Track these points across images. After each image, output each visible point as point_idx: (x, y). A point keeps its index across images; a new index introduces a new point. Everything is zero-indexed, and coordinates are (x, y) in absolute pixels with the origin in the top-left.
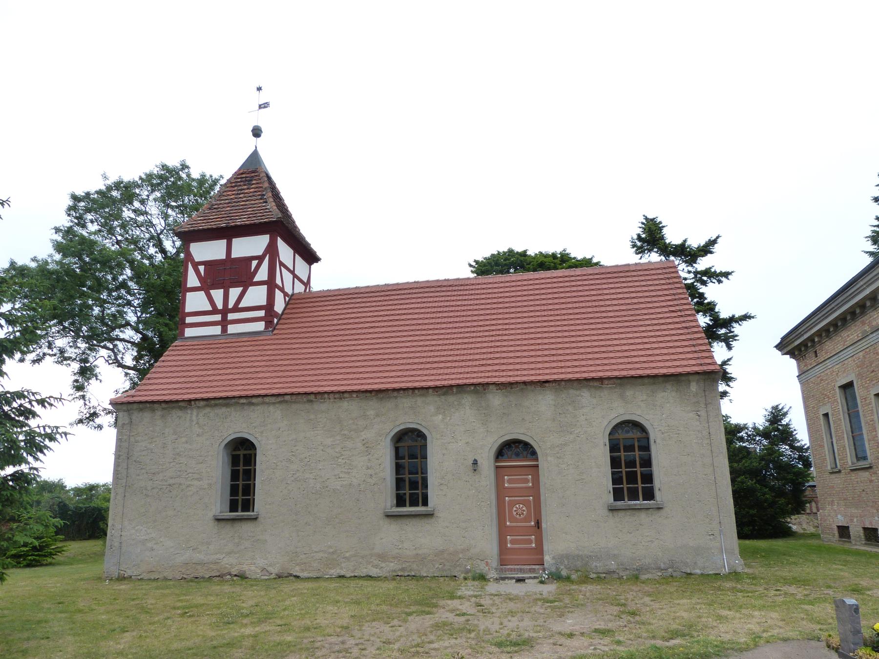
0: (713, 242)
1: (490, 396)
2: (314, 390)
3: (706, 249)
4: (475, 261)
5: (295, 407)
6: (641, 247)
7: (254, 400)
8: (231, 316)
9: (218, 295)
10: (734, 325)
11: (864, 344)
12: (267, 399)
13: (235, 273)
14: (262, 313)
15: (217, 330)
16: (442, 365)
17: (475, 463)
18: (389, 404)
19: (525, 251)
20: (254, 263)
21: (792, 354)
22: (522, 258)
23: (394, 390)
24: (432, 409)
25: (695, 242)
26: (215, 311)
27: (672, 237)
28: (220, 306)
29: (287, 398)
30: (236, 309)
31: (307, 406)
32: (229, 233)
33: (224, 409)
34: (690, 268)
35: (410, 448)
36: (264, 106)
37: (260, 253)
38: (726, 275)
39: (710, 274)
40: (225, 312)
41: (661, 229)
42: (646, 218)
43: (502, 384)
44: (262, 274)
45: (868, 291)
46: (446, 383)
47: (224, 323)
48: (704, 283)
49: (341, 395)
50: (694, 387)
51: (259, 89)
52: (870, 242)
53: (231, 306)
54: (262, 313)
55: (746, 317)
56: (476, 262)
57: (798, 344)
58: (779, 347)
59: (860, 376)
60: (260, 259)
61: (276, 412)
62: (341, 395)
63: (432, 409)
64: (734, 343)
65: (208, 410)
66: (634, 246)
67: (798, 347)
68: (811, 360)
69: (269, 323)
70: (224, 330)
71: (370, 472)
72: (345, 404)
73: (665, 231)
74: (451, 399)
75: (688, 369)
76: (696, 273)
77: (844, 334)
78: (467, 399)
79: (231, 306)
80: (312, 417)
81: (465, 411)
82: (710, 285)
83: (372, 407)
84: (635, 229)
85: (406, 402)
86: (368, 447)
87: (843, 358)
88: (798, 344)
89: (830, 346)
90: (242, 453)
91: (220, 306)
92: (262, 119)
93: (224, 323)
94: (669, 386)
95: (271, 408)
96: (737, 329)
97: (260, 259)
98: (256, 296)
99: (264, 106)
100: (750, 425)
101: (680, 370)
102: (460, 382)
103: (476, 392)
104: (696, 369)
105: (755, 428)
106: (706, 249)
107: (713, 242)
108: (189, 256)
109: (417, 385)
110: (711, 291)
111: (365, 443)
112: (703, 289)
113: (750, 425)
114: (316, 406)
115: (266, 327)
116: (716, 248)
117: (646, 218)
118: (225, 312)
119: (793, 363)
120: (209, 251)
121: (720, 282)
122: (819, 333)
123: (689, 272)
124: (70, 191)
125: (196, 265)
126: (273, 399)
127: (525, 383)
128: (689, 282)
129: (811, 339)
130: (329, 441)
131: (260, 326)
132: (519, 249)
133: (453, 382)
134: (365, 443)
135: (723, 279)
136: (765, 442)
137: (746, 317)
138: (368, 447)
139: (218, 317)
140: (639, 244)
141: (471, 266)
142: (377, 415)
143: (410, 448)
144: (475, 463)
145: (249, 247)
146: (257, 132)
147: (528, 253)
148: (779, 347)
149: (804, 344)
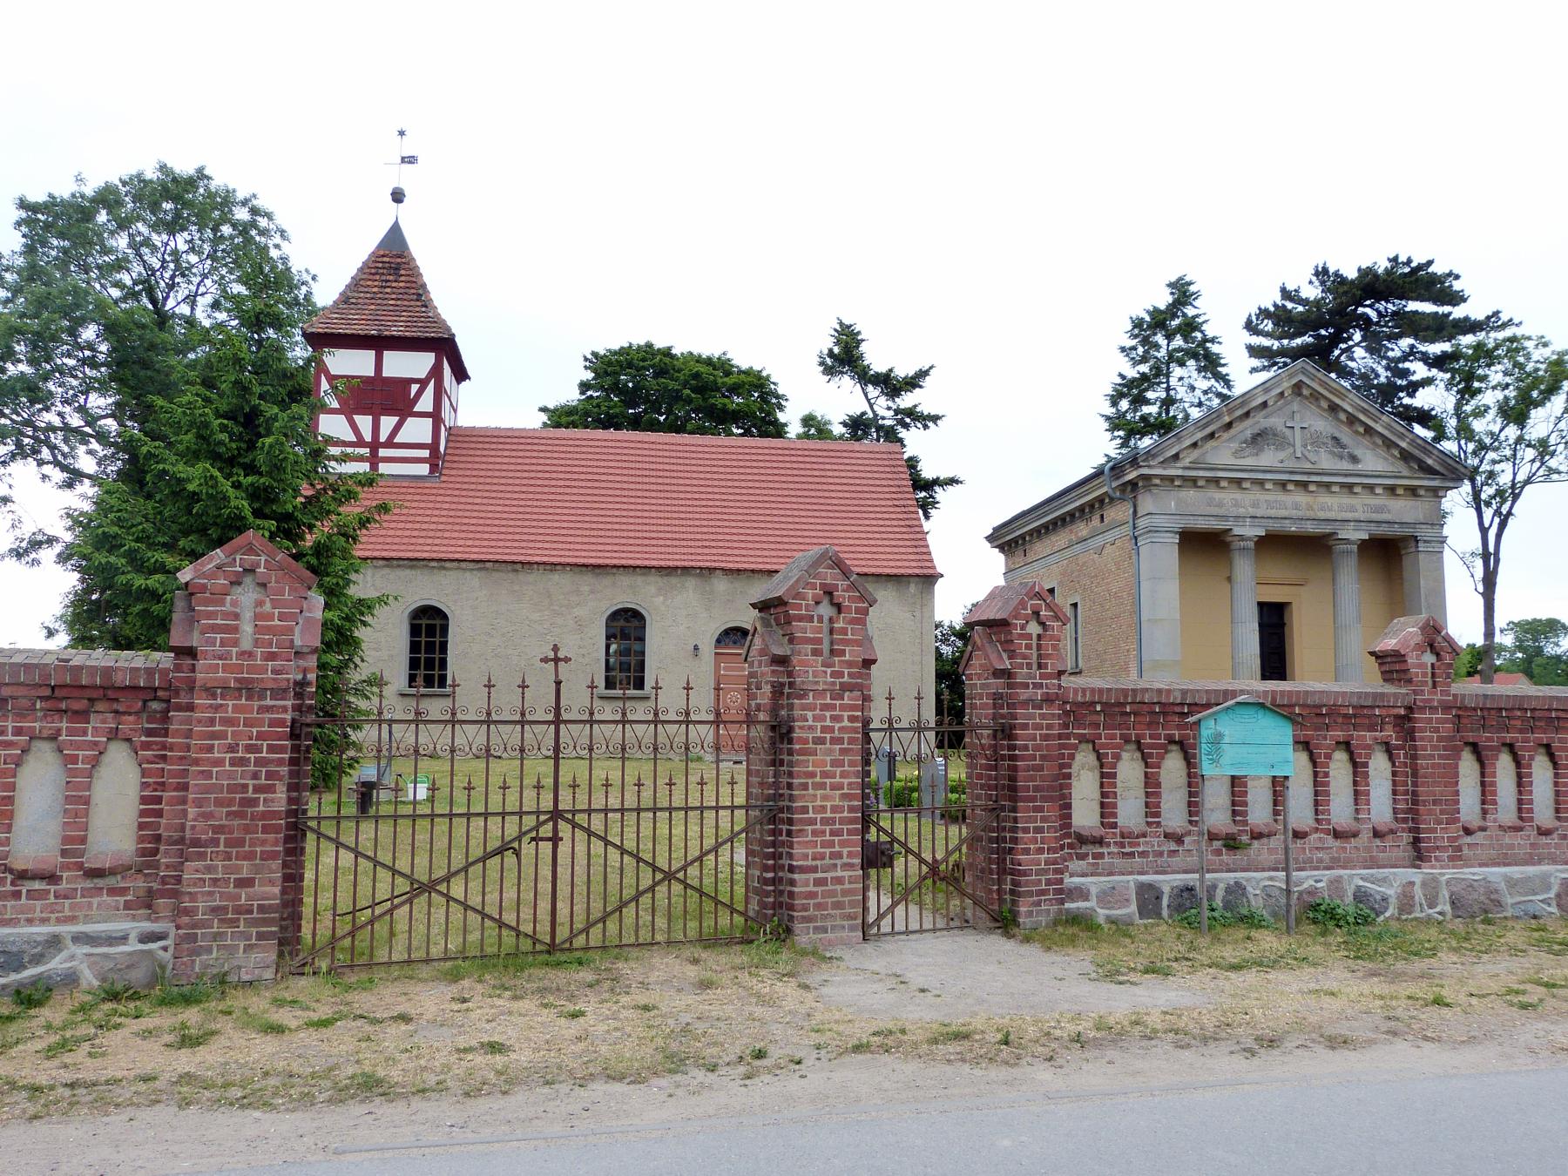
0: (923, 374)
1: (715, 581)
2: (521, 558)
3: (913, 383)
4: (593, 353)
5: (496, 575)
6: (832, 367)
7: (448, 565)
8: (382, 452)
9: (364, 422)
10: (937, 488)
11: (1067, 553)
12: (463, 565)
13: (388, 397)
14: (426, 453)
15: (364, 467)
16: (661, 542)
17: (696, 648)
18: (607, 581)
19: (670, 348)
20: (415, 388)
21: (1001, 548)
22: (667, 360)
23: (614, 566)
24: (653, 589)
25: (903, 371)
26: (360, 442)
27: (876, 358)
28: (368, 438)
29: (488, 565)
30: (390, 444)
31: (511, 575)
32: (379, 344)
33: (408, 571)
34: (890, 404)
35: (627, 627)
36: (409, 160)
37: (423, 376)
38: (935, 419)
39: (913, 416)
40: (375, 445)
41: (859, 342)
42: (841, 324)
43: (730, 570)
44: (426, 403)
45: (1077, 504)
46: (671, 564)
47: (374, 460)
48: (906, 426)
49: (553, 566)
50: (913, 588)
51: (402, 133)
52: (1108, 403)
53: (383, 439)
54: (426, 453)
55: (952, 481)
56: (595, 354)
57: (1011, 539)
58: (990, 539)
59: (1061, 583)
60: (423, 383)
61: (473, 580)
62: (553, 566)
63: (653, 589)
64: (932, 512)
65: (387, 570)
66: (821, 364)
67: (1009, 543)
68: (1019, 559)
69: (434, 468)
70: (374, 467)
71: (582, 651)
72: (556, 577)
73: (863, 348)
74: (674, 580)
75: (910, 571)
76: (897, 412)
77: (1054, 538)
78: (691, 582)
79: (383, 439)
80: (517, 588)
81: (688, 593)
82: (913, 429)
83: (586, 582)
84: (827, 343)
85: (625, 580)
86: (580, 625)
87: (1049, 563)
88: (1011, 539)
89: (1041, 548)
90: (424, 622)
91: (368, 438)
92: (406, 178)
93: (374, 460)
94: (890, 585)
95: (468, 574)
96: (940, 493)
97: (423, 383)
98: (417, 430)
99: (409, 160)
100: (946, 624)
101: (902, 571)
102: (686, 564)
103: (701, 575)
104: (917, 571)
105: (951, 627)
106: (913, 383)
107: (923, 374)
108: (322, 369)
109: (639, 563)
110: (915, 441)
111: (577, 620)
112: (903, 433)
113: (946, 624)
114: (521, 576)
115: (432, 471)
116: (928, 382)
117: (841, 324)
118: (375, 445)
119: (1002, 557)
120: (352, 363)
121: (926, 427)
122: (1031, 533)
123: (889, 408)
124: (18, 195)
125: (332, 379)
126: (471, 565)
127: (753, 571)
128: (888, 423)
129: (1022, 537)
130: (536, 616)
131: (424, 469)
132: (659, 344)
133: (679, 564)
134: (577, 620)
135: (930, 424)
136: (959, 644)
137: (952, 481)
138: (580, 625)
139: (365, 451)
140: (829, 361)
141: (586, 359)
142: (592, 592)
143: (627, 627)
144: (696, 648)
145: (400, 365)
146: (398, 196)
147: (674, 351)
148: (990, 539)
149: (1015, 540)
